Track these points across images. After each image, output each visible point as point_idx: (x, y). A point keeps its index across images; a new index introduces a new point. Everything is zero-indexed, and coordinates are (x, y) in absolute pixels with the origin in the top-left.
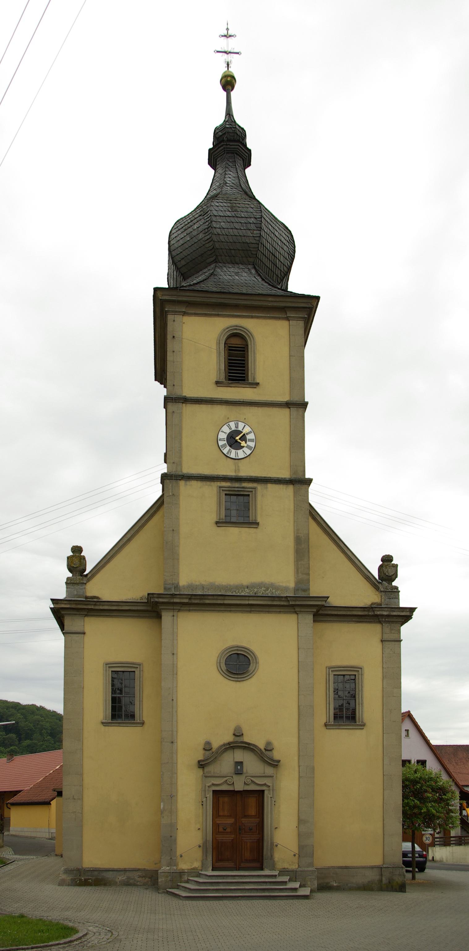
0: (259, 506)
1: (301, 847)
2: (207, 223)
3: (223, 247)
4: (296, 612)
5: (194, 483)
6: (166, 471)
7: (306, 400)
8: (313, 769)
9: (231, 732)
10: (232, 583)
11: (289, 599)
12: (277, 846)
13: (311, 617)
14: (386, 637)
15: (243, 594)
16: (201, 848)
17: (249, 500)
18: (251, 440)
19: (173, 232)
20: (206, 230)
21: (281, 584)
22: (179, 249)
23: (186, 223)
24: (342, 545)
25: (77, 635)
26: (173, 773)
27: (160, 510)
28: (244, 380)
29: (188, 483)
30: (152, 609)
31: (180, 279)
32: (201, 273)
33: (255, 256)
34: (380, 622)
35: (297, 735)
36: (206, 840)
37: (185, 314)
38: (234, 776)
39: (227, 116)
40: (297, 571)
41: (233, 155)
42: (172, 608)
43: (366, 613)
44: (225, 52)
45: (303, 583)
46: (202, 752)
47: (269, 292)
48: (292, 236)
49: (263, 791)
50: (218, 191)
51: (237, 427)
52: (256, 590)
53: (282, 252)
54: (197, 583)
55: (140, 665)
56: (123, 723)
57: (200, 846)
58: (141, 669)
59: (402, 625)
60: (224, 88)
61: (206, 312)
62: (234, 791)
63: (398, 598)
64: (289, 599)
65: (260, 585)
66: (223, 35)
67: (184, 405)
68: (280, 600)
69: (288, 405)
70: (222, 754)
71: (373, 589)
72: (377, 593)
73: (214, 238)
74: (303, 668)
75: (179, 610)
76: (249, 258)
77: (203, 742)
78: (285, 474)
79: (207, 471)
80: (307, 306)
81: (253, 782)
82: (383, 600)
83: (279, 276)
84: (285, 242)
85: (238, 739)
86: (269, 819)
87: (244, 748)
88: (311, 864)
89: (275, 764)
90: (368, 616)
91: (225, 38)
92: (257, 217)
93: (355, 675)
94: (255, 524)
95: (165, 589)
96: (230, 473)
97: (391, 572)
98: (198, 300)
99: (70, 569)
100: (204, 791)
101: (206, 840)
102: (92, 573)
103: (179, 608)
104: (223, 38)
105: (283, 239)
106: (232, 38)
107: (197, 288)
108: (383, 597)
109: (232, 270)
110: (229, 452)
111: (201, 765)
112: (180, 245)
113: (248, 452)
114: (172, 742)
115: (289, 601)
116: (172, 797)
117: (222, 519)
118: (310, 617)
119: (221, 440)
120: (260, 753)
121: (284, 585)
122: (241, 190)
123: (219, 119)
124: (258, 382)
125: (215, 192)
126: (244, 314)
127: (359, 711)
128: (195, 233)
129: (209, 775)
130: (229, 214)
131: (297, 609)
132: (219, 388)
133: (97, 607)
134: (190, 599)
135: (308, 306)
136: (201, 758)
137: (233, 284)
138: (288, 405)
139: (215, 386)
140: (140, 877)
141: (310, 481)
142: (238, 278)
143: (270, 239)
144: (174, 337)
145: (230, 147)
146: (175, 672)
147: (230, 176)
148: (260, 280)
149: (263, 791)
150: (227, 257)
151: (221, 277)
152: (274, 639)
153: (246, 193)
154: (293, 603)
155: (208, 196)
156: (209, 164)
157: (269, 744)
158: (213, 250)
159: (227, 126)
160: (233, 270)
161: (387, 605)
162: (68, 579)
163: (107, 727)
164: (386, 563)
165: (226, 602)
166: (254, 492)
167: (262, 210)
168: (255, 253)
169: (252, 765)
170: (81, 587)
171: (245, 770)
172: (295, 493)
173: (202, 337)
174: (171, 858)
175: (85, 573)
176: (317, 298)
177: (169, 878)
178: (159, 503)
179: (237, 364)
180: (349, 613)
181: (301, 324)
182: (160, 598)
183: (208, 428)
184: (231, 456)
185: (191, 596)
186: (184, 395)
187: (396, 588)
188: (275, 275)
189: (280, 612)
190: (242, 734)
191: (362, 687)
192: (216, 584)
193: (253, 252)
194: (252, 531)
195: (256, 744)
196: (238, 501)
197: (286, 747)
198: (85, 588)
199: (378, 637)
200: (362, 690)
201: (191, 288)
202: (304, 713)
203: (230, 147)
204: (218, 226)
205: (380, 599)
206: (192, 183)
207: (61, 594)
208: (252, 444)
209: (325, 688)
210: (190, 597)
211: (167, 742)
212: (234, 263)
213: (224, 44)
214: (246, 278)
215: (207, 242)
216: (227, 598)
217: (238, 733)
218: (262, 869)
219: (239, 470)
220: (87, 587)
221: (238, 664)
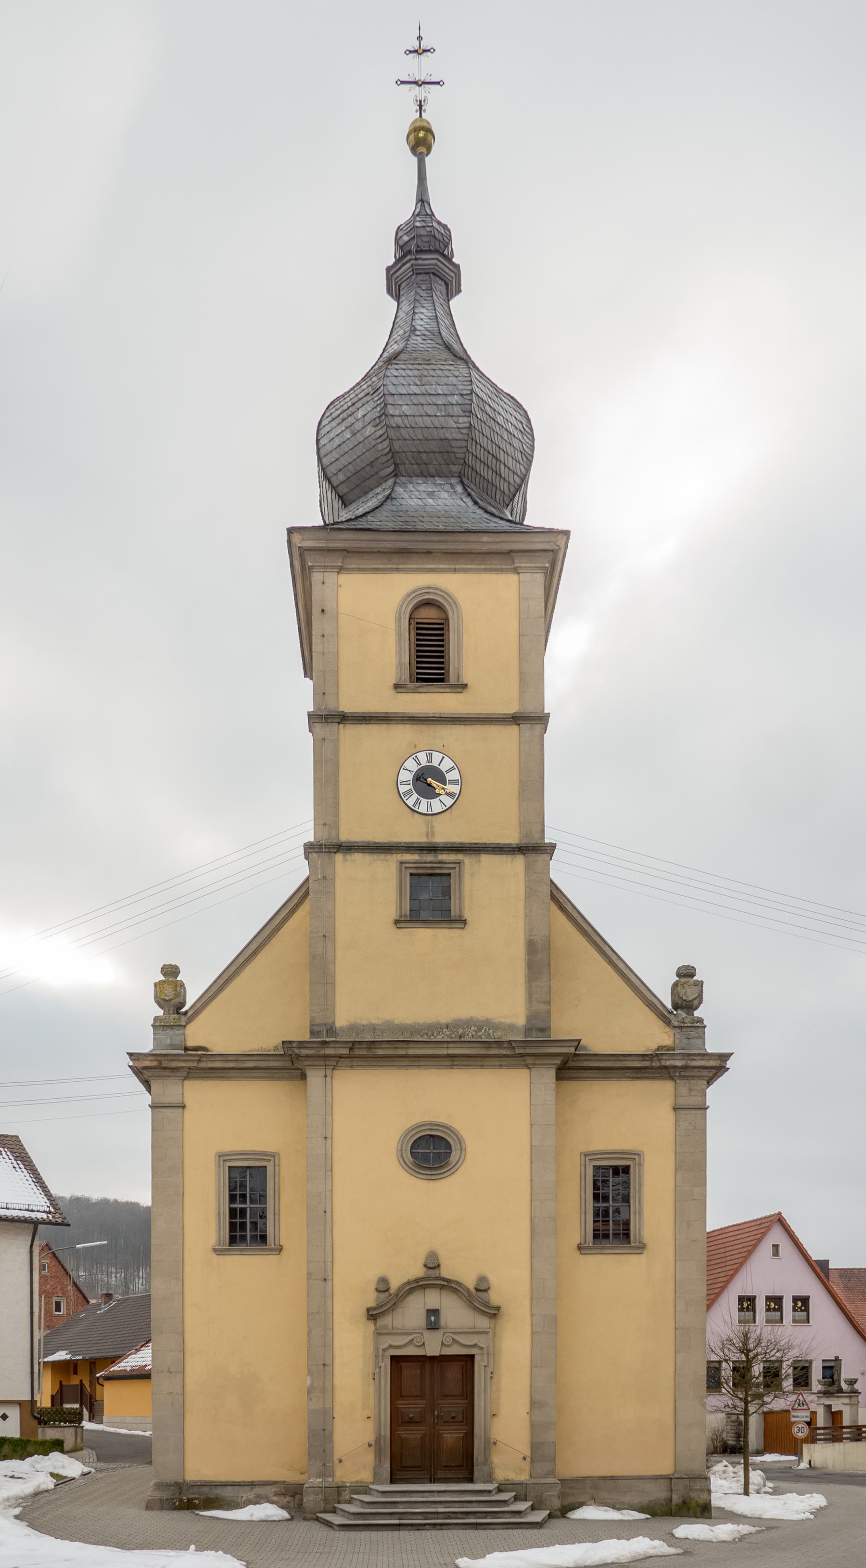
0: (466, 892)
1: (535, 1446)
2: (379, 409)
4: (527, 1066)
5: (358, 857)
6: (312, 840)
9: (421, 1262)
10: (421, 1021)
12: (495, 1443)
13: (552, 1073)
14: (682, 1101)
15: (439, 1038)
16: (372, 1449)
17: (450, 883)
18: (453, 782)
19: (323, 423)
21: (503, 1020)
22: (334, 453)
23: (345, 407)
28: (442, 680)
29: (348, 857)
31: (337, 504)
32: (370, 495)
34: (671, 1078)
35: (528, 1265)
36: (380, 1435)
37: (341, 570)
39: (419, 205)
41: (427, 277)
43: (647, 1064)
44: (415, 83)
45: (539, 1024)
46: (375, 1294)
47: (484, 526)
48: (529, 420)
49: (472, 1357)
50: (402, 346)
52: (461, 1031)
53: (510, 450)
54: (365, 1022)
55: (274, 1155)
57: (370, 1445)
58: (277, 1163)
59: (709, 1082)
60: (414, 150)
61: (377, 566)
62: (425, 1356)
63: (702, 1037)
64: (514, 1045)
65: (468, 1023)
66: (412, 49)
67: (341, 726)
68: (501, 1048)
72: (668, 1029)
73: (392, 434)
76: (451, 466)
77: (374, 1280)
78: (512, 837)
79: (381, 837)
82: (677, 1042)
83: (507, 492)
84: (515, 432)
85: (433, 1273)
86: (483, 1400)
87: (442, 1287)
88: (552, 1473)
89: (493, 1313)
90: (652, 1068)
91: (415, 54)
92: (465, 392)
94: (461, 922)
95: (312, 1033)
96: (418, 837)
97: (690, 994)
98: (363, 545)
99: (161, 1002)
101: (380, 1435)
102: (196, 1008)
104: (411, 55)
105: (511, 429)
106: (428, 54)
107: (362, 524)
108: (678, 1036)
109: (422, 488)
110: (417, 802)
111: (372, 1315)
113: (449, 801)
114: (325, 1280)
117: (405, 916)
118: (550, 1074)
119: (402, 783)
120: (466, 1295)
122: (440, 341)
124: (465, 682)
125: (395, 347)
126: (441, 566)
127: (635, 1224)
128: (359, 425)
129: (384, 1331)
130: (415, 389)
131: (529, 1061)
132: (399, 695)
135: (550, 548)
136: (372, 1304)
137: (424, 515)
138: (516, 719)
140: (276, 1494)
142: (434, 500)
143: (488, 430)
144: (323, 611)
145: (424, 261)
147: (422, 316)
148: (470, 503)
149: (472, 1357)
150: (415, 466)
151: (404, 502)
152: (493, 1111)
153: (448, 347)
154: (521, 1051)
155: (386, 355)
157: (482, 1279)
159: (418, 224)
160: (423, 487)
161: (683, 1049)
162: (156, 1019)
164: (683, 980)
165: (411, 1052)
166: (457, 869)
167: (474, 380)
168: (462, 456)
169: (456, 1314)
170: (178, 1032)
171: (442, 1322)
172: (527, 868)
173: (374, 604)
175: (183, 1010)
177: (321, 1497)
179: (430, 652)
180: (618, 1064)
182: (303, 1048)
183: (381, 762)
185: (353, 1045)
186: (341, 710)
187: (700, 1020)
188: (498, 492)
189: (501, 1065)
190: (439, 1266)
191: (640, 1185)
192: (396, 1022)
193: (458, 455)
194: (455, 933)
195: (461, 1281)
196: (431, 891)
197: (511, 1285)
198: (184, 1034)
200: (640, 1190)
201: (350, 525)
203: (424, 261)
204: (397, 413)
205: (672, 1039)
206: (358, 328)
207: (146, 1044)
208: (455, 789)
209: (578, 1188)
211: (320, 1278)
212: (426, 475)
213: (413, 68)
214: (447, 502)
215: (379, 441)
216: (411, 1045)
217: (432, 1264)
218: (471, 1480)
219: (433, 834)
220: (186, 1032)
221: (431, 1152)
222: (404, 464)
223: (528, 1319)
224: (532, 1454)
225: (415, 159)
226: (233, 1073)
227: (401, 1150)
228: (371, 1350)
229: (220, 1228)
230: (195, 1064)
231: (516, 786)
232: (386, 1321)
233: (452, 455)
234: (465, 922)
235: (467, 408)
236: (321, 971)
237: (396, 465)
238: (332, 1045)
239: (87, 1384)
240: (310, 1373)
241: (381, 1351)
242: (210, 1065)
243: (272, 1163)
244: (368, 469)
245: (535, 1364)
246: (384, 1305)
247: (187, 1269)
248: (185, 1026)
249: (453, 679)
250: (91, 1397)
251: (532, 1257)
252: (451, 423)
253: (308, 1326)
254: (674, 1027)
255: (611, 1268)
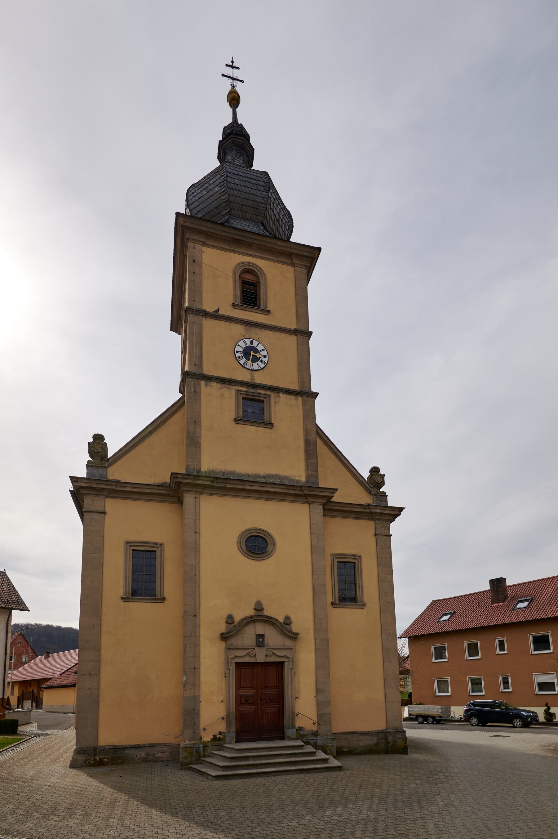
1: (320, 716)
3: (236, 202)
4: (308, 503)
7: (310, 330)
8: (328, 641)
9: (252, 606)
11: (303, 488)
14: (379, 532)
16: (224, 721)
20: (222, 184)
24: (340, 455)
25: (97, 514)
26: (197, 646)
27: (181, 409)
30: (175, 491)
33: (263, 215)
34: (373, 520)
36: (229, 712)
37: (204, 244)
38: (256, 648)
40: (307, 469)
42: (195, 490)
43: (363, 510)
49: (282, 663)
51: (252, 343)
55: (161, 545)
56: (144, 599)
58: (163, 549)
64: (303, 488)
67: (204, 318)
69: (295, 332)
70: (244, 627)
71: (366, 492)
72: (369, 496)
74: (316, 550)
75: (201, 493)
76: (258, 217)
77: (225, 616)
78: (295, 387)
80: (309, 256)
81: (273, 654)
87: (265, 622)
89: (294, 637)
93: (354, 563)
94: (270, 425)
99: (91, 455)
100: (227, 663)
101: (229, 712)
103: (201, 490)
104: (228, 67)
111: (224, 638)
112: (197, 198)
113: (262, 366)
115: (303, 491)
116: (196, 669)
119: (237, 352)
121: (297, 478)
123: (229, 120)
126: (257, 254)
133: (118, 489)
134: (212, 482)
136: (223, 630)
138: (295, 332)
139: (232, 308)
141: (316, 394)
146: (198, 550)
149: (282, 663)
152: (289, 524)
156: (218, 158)
157: (287, 618)
158: (227, 203)
162: (88, 462)
163: (127, 603)
165: (247, 487)
168: (264, 212)
169: (273, 638)
171: (266, 643)
172: (304, 404)
174: (194, 732)
176: (319, 249)
178: (180, 403)
179: (250, 293)
181: (305, 271)
184: (247, 367)
189: (294, 501)
190: (263, 609)
196: (254, 405)
199: (373, 531)
202: (317, 591)
210: (212, 479)
211: (191, 615)
213: (229, 71)
215: (222, 194)
216: (247, 483)
217: (259, 607)
218: (283, 738)
222: (234, 209)
223: (313, 642)
224: (318, 720)
225: (231, 110)
226: (136, 496)
227: (240, 543)
228: (223, 659)
229: (126, 586)
230: (114, 488)
231: (296, 364)
232: (233, 641)
233: (259, 210)
234: (272, 425)
235: (267, 189)
236: (193, 442)
237: (231, 209)
238: (201, 478)
239: (35, 691)
240: (185, 673)
241: (230, 660)
242: (123, 489)
243: (159, 549)
244: (215, 210)
245: (318, 668)
246: (231, 631)
247: (104, 610)
248: (107, 468)
249: (262, 307)
250: (37, 697)
251: (314, 606)
252: (259, 193)
253: (184, 644)
254: (373, 495)
255: (346, 616)
